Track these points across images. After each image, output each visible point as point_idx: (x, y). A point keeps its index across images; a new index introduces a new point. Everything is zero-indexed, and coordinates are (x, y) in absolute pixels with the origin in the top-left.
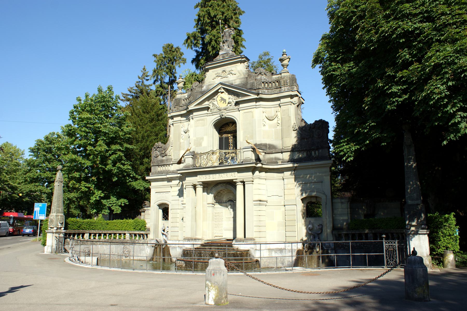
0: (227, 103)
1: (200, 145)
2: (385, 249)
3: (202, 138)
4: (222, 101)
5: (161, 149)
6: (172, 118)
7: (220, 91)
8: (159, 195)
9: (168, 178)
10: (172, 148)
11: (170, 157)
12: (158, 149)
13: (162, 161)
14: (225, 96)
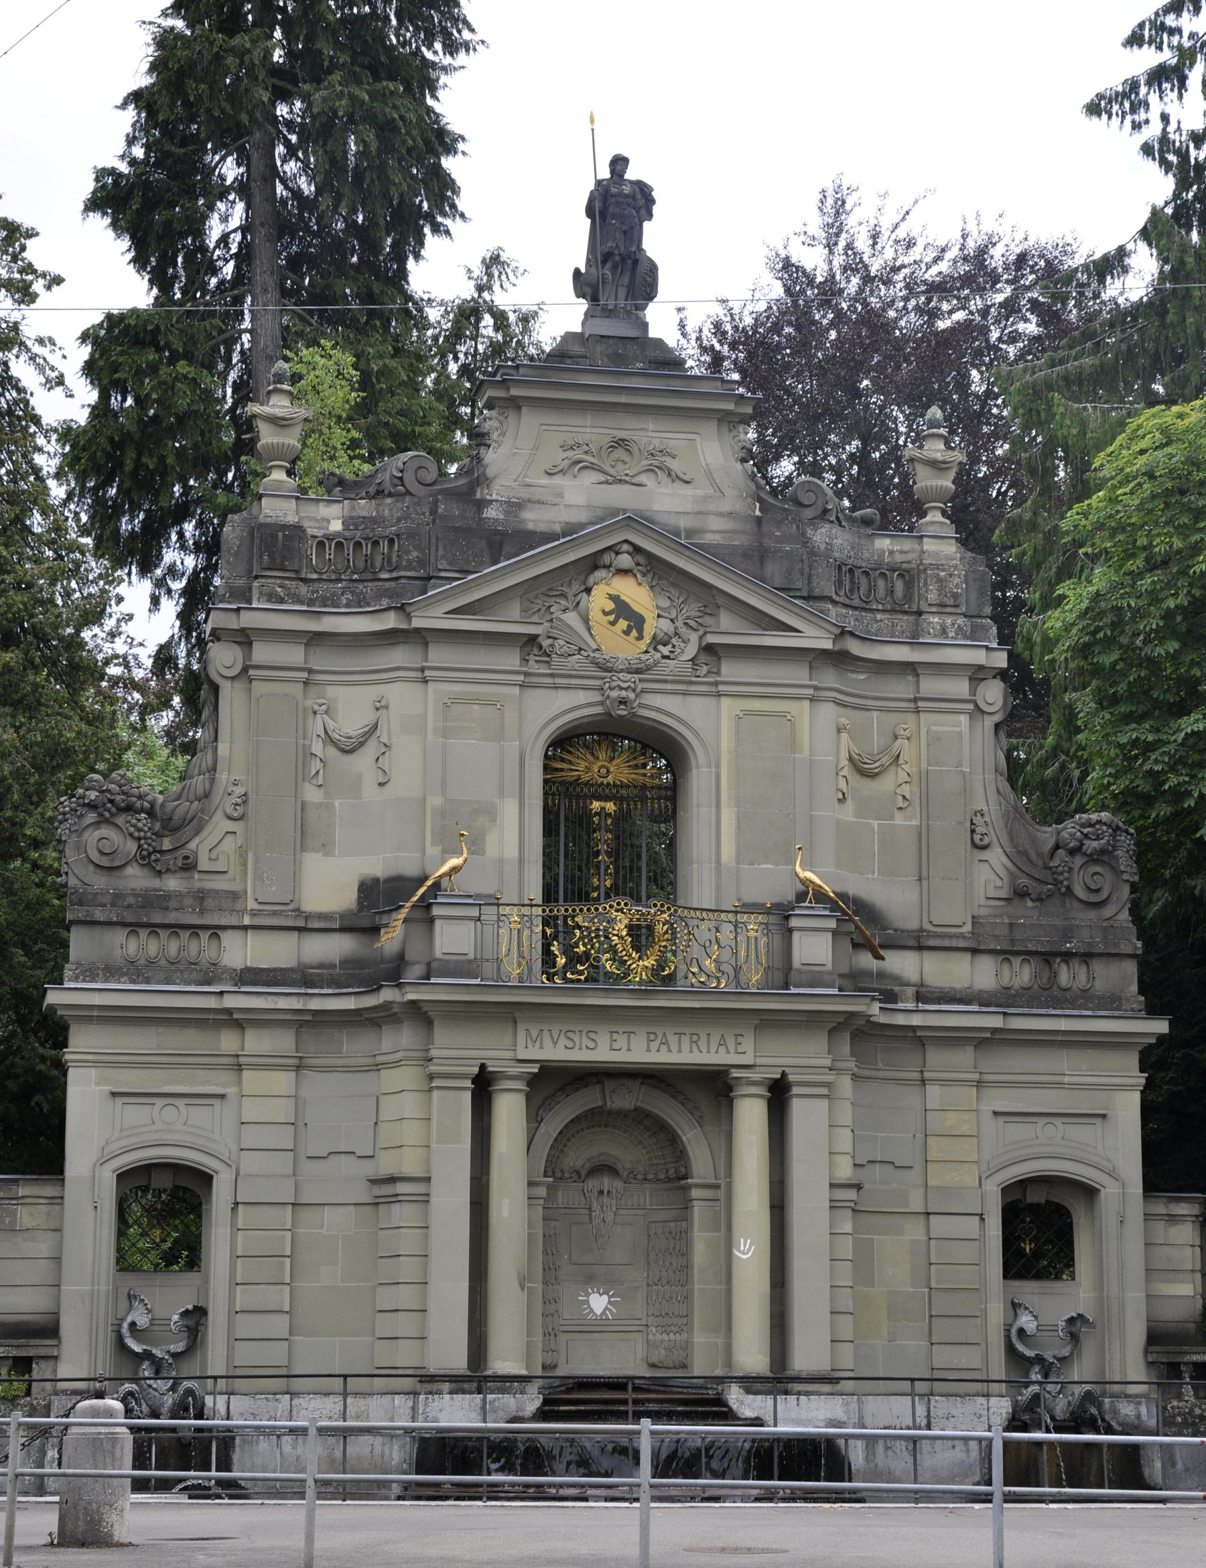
0: (647, 639)
2: (776, 1460)
3: (491, 812)
4: (623, 624)
6: (244, 638)
8: (136, 1114)
9: (229, 1011)
12: (121, 820)
13: (160, 900)
14: (637, 594)
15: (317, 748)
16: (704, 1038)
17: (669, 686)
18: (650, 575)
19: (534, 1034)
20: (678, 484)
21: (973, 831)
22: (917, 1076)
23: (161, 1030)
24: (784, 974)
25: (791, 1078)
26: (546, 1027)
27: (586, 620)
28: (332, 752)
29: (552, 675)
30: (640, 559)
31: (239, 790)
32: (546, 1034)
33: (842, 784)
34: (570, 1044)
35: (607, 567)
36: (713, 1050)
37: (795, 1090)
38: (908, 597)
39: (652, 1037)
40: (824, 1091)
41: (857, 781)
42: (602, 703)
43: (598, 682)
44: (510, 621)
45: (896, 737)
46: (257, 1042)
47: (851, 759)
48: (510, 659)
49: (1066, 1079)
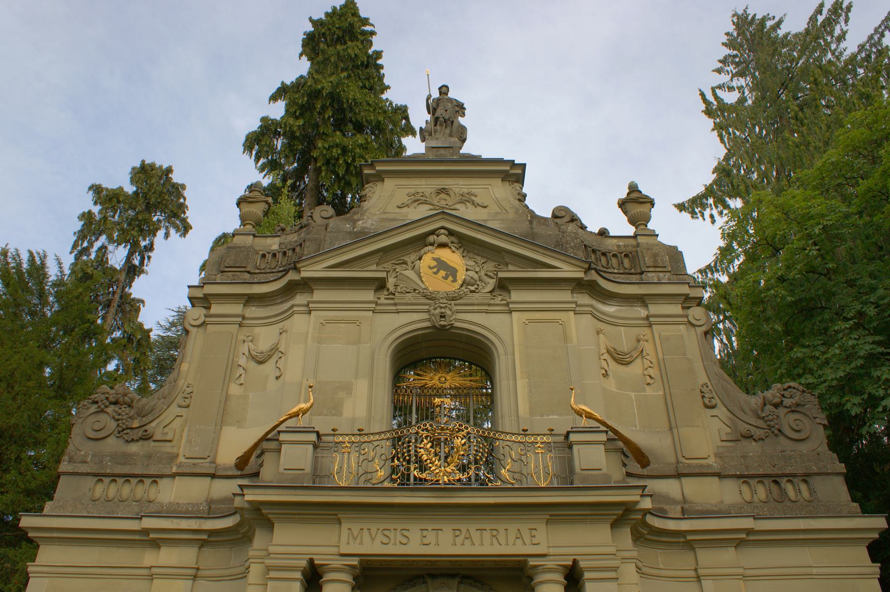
0: (460, 282)
1: (336, 409)
3: (348, 388)
4: (442, 273)
5: (125, 410)
7: (431, 238)
9: (146, 532)
10: (183, 412)
11: (167, 448)
12: (110, 409)
13: (127, 458)
14: (453, 257)
15: (242, 361)
16: (502, 532)
17: (475, 308)
18: (462, 250)
19: (356, 532)
20: (478, 208)
21: (703, 397)
22: (692, 573)
23: (103, 549)
24: (567, 477)
25: (582, 564)
26: (366, 526)
27: (419, 275)
28: (253, 364)
29: (395, 304)
30: (453, 239)
31: (189, 390)
32: (365, 532)
33: (604, 364)
34: (385, 540)
35: (432, 244)
36: (511, 542)
37: (587, 575)
38: (633, 266)
39: (457, 533)
40: (612, 575)
41: (613, 366)
42: (429, 320)
43: (427, 307)
44: (371, 271)
45: (638, 341)
46: (168, 556)
47: (608, 352)
48: (368, 295)
49: (815, 571)
